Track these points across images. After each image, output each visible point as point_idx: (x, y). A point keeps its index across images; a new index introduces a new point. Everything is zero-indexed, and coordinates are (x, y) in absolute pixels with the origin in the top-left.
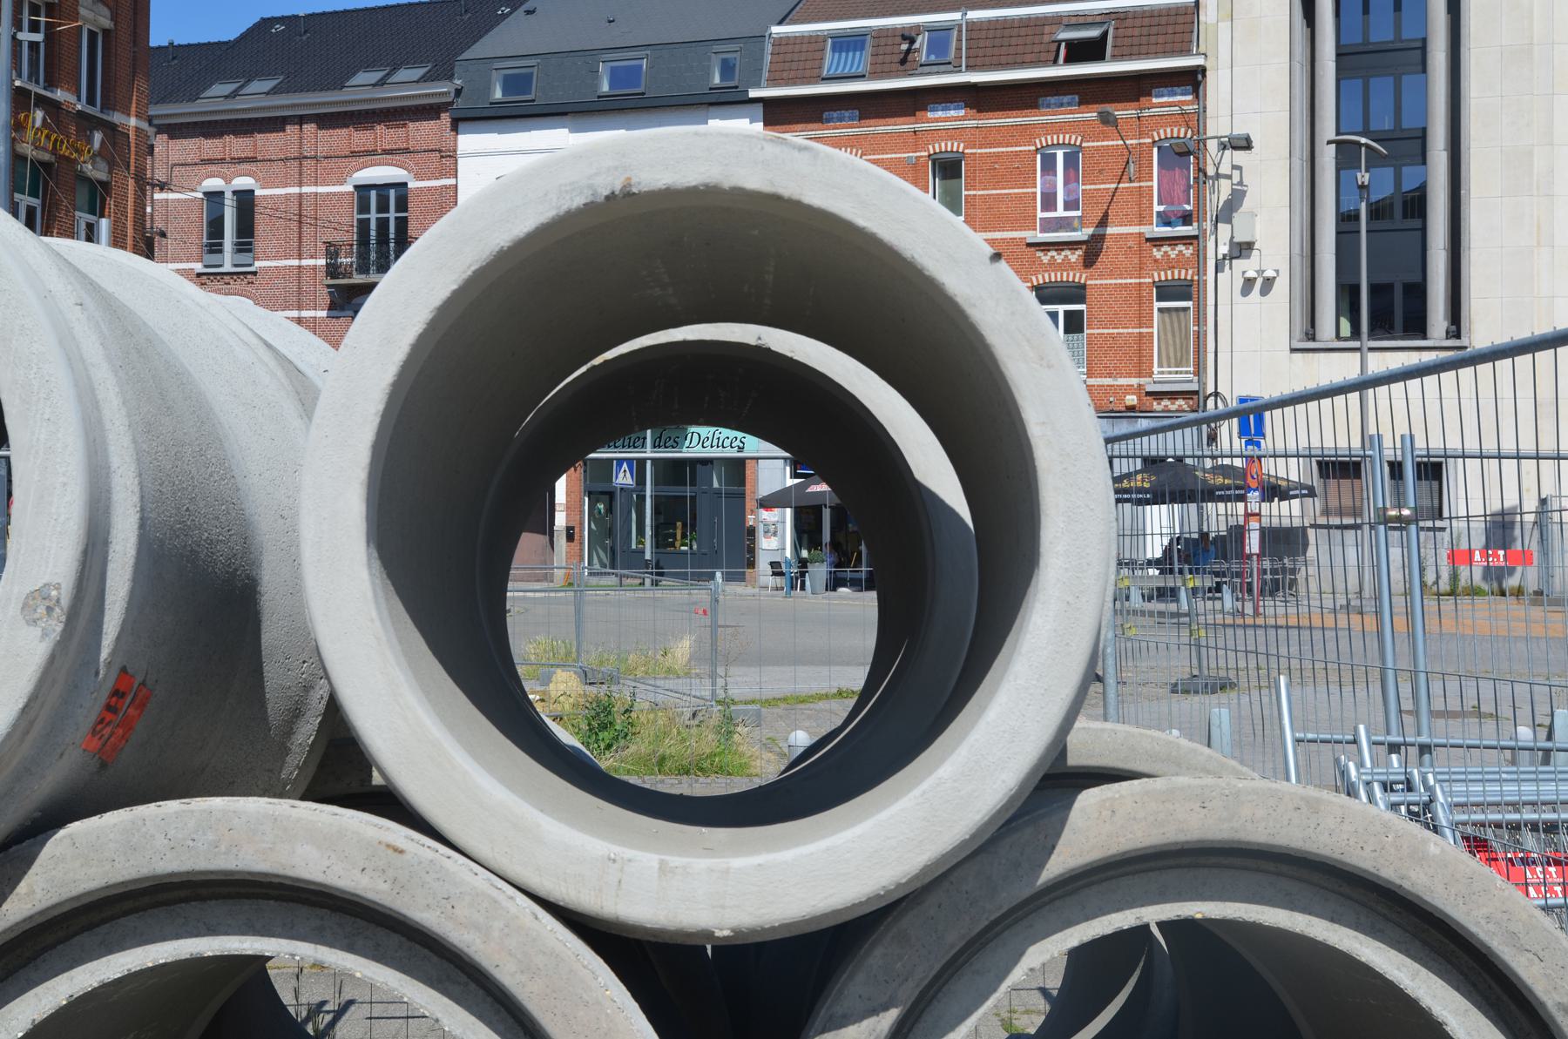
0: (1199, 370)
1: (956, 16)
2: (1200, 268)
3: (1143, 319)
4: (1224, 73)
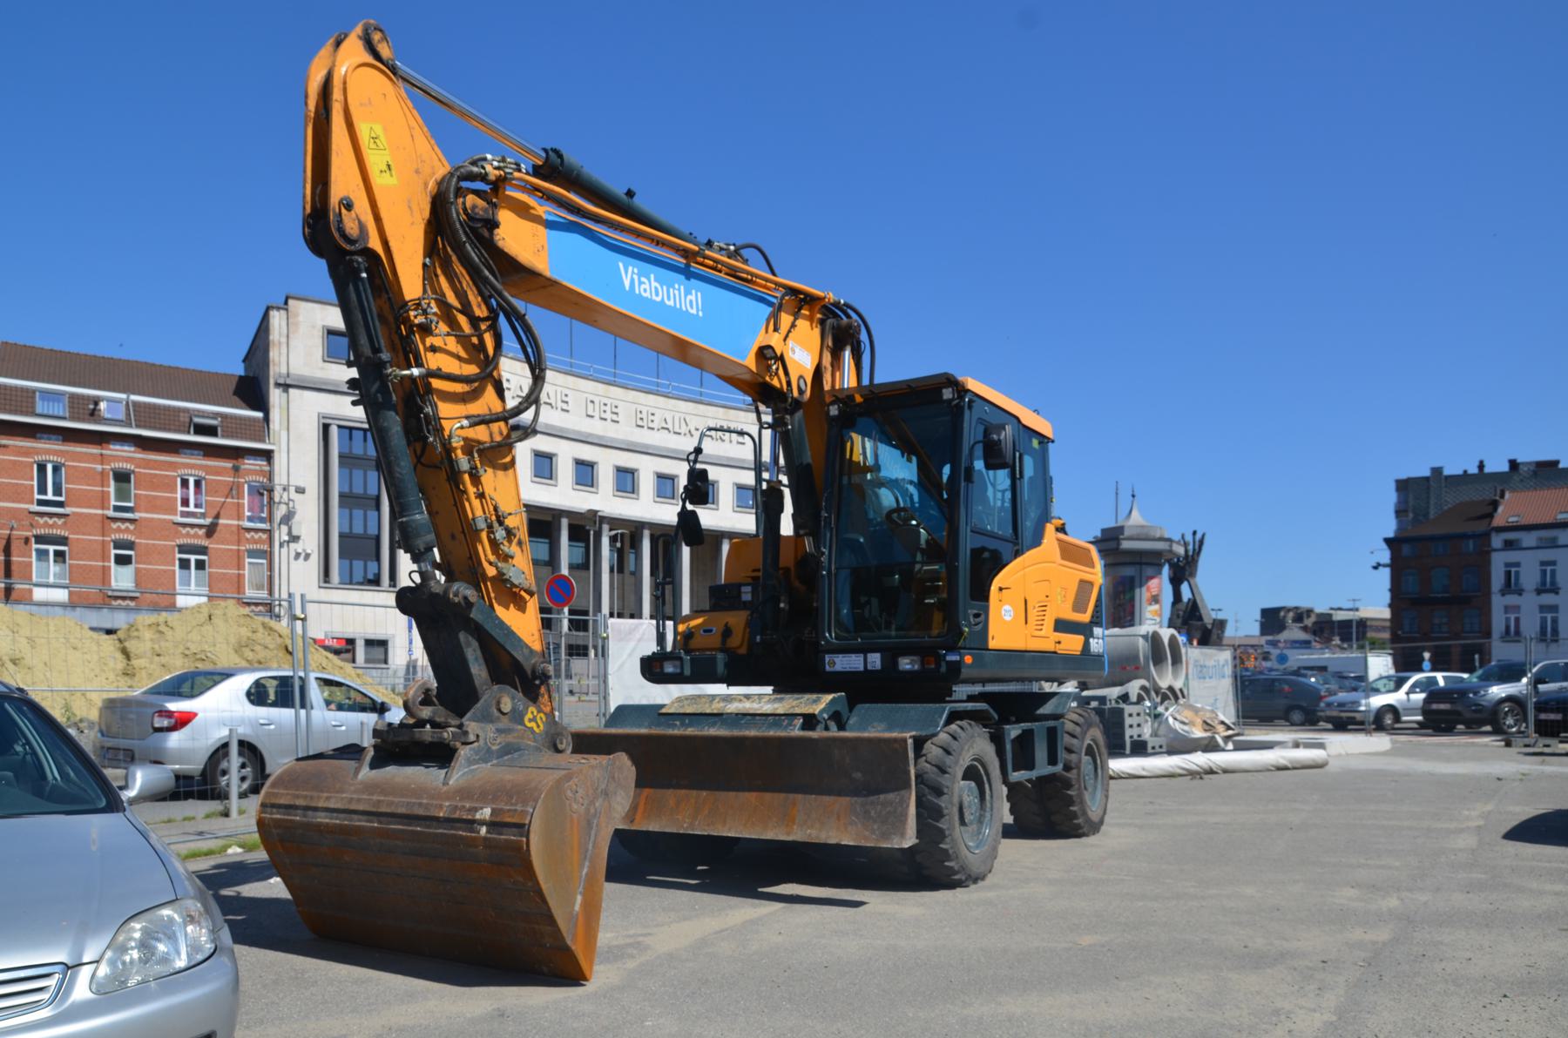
0: (271, 592)
1: (124, 396)
2: (271, 544)
3: (240, 566)
4: (284, 455)
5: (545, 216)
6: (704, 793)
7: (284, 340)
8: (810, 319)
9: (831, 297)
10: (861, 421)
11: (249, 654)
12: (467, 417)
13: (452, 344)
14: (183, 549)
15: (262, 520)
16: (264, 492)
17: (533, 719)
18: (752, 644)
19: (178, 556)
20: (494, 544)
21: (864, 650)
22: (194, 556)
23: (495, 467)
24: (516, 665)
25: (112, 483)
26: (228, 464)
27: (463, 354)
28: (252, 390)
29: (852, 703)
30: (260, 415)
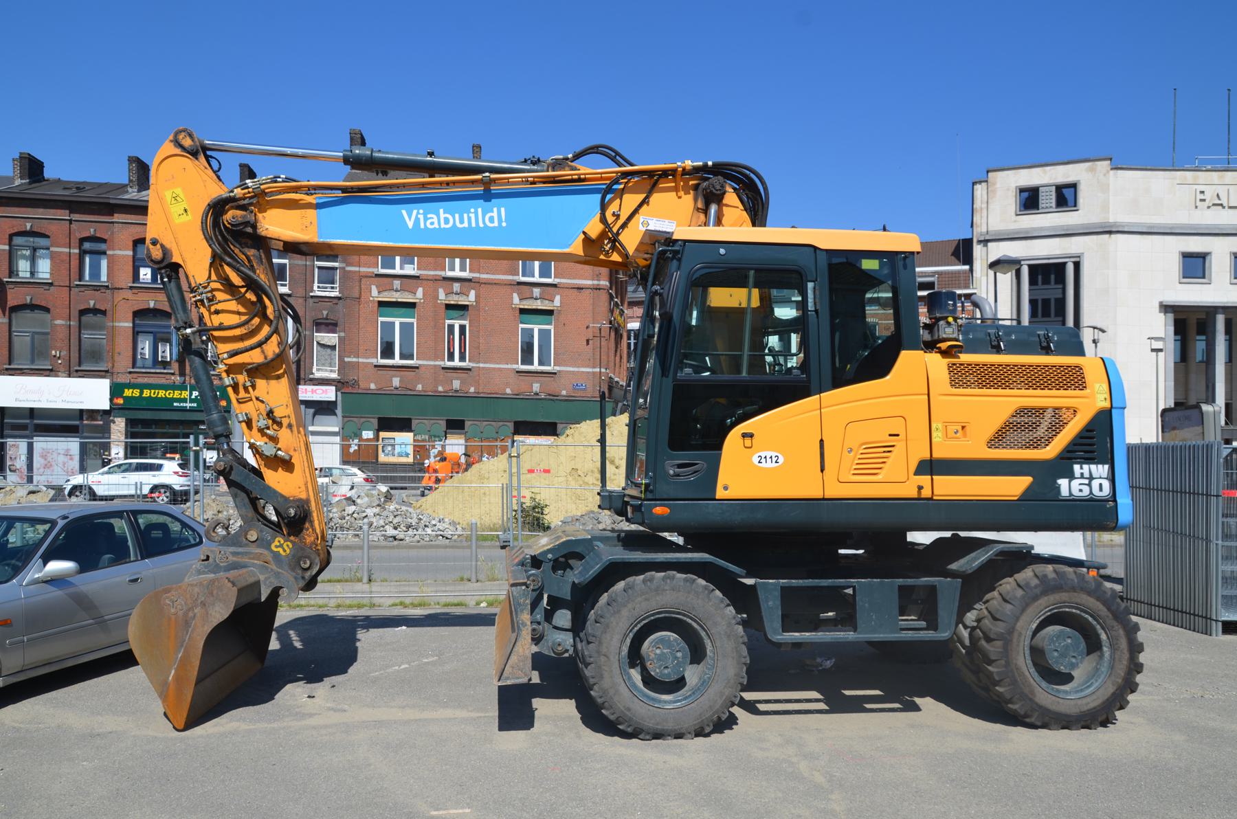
5: (314, 202)
7: (984, 206)
13: (233, 305)
17: (281, 546)
23: (267, 377)
27: (242, 310)
30: (967, 267)
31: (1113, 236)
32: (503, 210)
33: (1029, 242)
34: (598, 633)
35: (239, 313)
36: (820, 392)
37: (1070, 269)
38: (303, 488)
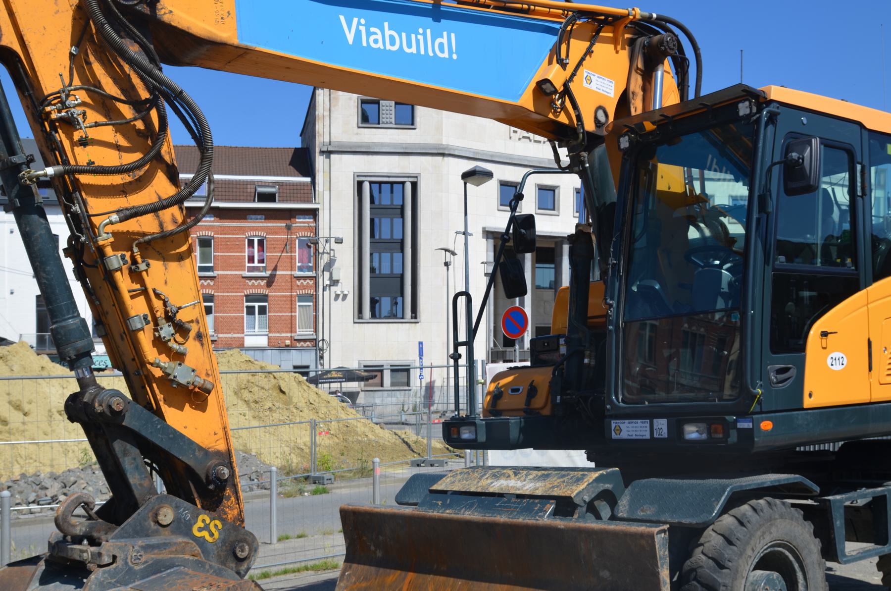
0: (316, 330)
3: (292, 310)
4: (327, 212)
6: (460, 582)
7: (327, 113)
8: (614, 41)
9: (638, 12)
10: (662, 149)
11: (246, 395)
12: (118, 212)
13: (108, 133)
14: (249, 298)
15: (309, 269)
16: (312, 244)
17: (206, 528)
18: (555, 405)
19: (246, 304)
20: (160, 344)
21: (649, 416)
22: (257, 304)
23: (165, 258)
24: (190, 472)
25: (198, 248)
26: (282, 224)
27: (123, 142)
28: (303, 161)
29: (628, 479)
30: (308, 179)
31: (446, 159)
32: (453, 35)
33: (370, 157)
34: (727, 581)
35: (118, 148)
36: (866, 287)
37: (408, 187)
38: (221, 433)
